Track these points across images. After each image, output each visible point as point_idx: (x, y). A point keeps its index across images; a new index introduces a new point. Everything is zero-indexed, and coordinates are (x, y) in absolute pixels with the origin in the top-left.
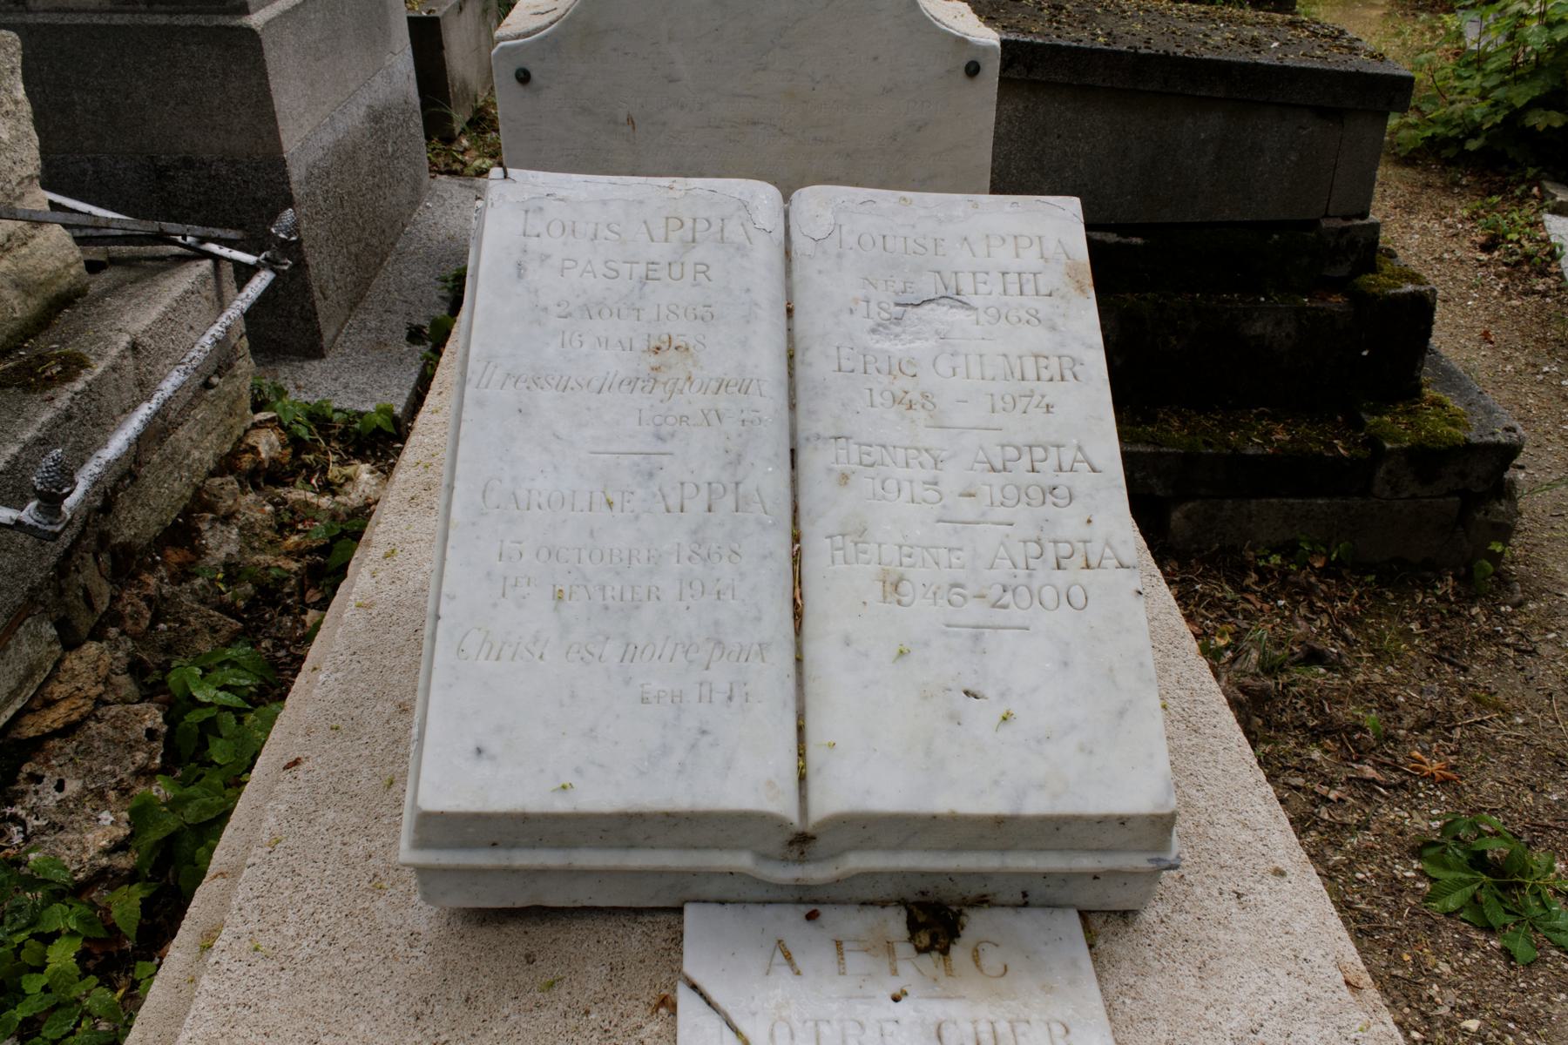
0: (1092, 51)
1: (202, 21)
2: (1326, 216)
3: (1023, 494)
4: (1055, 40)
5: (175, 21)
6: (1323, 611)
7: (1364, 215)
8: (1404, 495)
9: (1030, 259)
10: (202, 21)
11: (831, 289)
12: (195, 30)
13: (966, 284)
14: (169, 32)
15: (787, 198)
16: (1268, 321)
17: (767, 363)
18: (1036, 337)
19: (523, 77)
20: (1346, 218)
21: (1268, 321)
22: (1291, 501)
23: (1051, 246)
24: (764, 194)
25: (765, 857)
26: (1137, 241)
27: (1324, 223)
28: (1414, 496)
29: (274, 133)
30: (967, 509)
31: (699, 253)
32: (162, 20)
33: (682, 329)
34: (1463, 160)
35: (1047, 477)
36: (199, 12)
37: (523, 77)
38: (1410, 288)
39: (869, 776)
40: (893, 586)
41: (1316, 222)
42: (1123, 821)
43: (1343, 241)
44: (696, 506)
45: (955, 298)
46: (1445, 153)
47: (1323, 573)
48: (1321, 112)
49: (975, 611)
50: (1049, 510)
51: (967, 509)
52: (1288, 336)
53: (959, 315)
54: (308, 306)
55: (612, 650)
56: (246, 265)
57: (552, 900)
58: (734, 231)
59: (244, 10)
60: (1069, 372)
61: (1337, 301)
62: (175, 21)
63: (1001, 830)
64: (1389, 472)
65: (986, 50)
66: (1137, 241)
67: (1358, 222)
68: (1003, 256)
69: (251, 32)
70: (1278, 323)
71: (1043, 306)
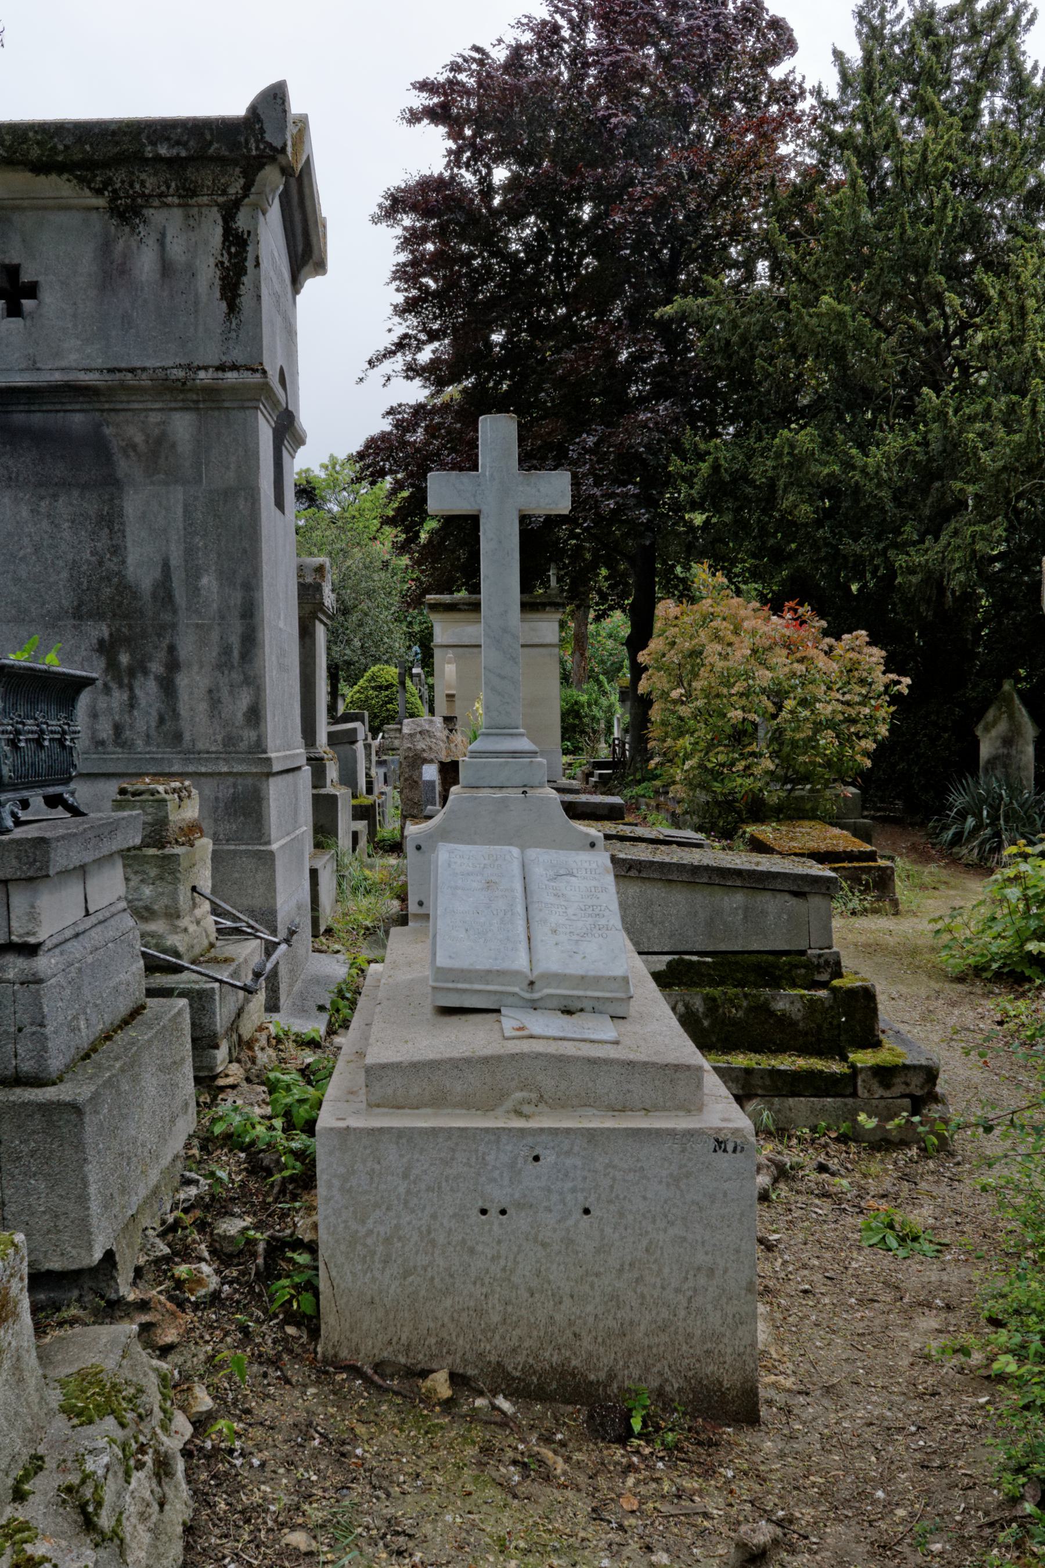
1: (250, 847)
3: (590, 915)
7: (830, 948)
9: (594, 866)
11: (538, 872)
12: (246, 852)
14: (235, 852)
16: (788, 1000)
18: (594, 883)
19: (419, 848)
21: (788, 1000)
24: (515, 851)
26: (709, 960)
28: (882, 1098)
29: (274, 898)
32: (233, 847)
33: (494, 879)
34: (998, 977)
35: (597, 911)
37: (419, 848)
40: (555, 932)
42: (615, 978)
43: (822, 961)
45: (572, 875)
46: (985, 975)
47: (837, 1140)
48: (796, 894)
49: (575, 937)
58: (508, 857)
61: (823, 993)
63: (583, 980)
66: (709, 960)
70: (792, 1003)
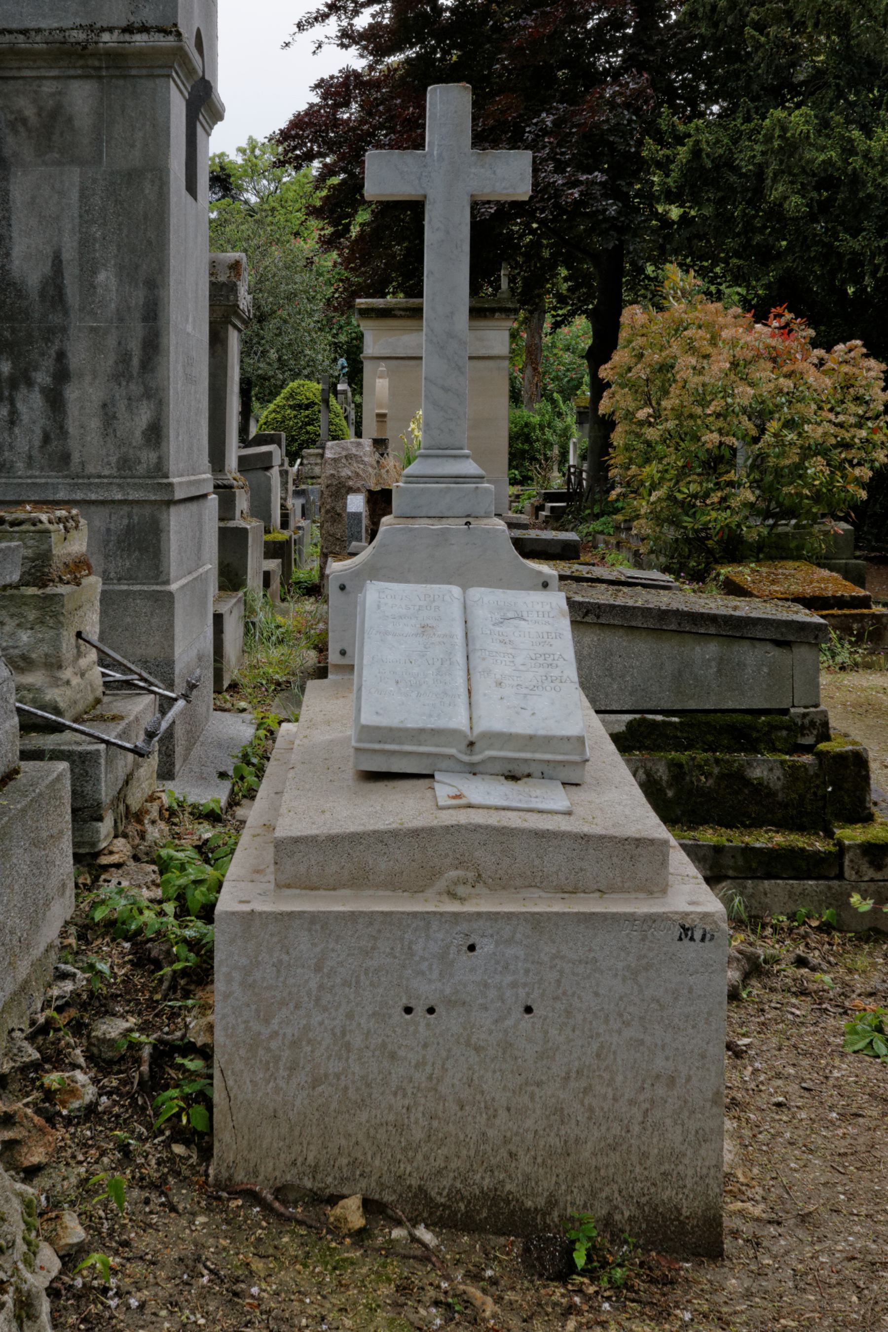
0: (634, 608)
1: (145, 588)
2: (793, 706)
3: (541, 665)
4: (612, 602)
5: (131, 588)
6: (815, 948)
7: (816, 706)
8: (866, 879)
9: (547, 608)
10: (145, 588)
11: (482, 616)
12: (140, 592)
13: (525, 615)
14: (128, 593)
15: (464, 592)
16: (764, 768)
17: (459, 632)
18: (547, 628)
19: (343, 588)
20: (806, 707)
21: (764, 768)
22: (791, 882)
23: (554, 605)
24: (456, 590)
25: (460, 752)
26: (676, 719)
27: (792, 710)
30: (522, 668)
31: (436, 604)
32: (125, 587)
35: (550, 661)
36: (144, 584)
37: (343, 588)
38: (850, 748)
39: (495, 717)
41: (788, 710)
42: (569, 739)
43: (806, 721)
44: (438, 664)
47: (819, 929)
48: (778, 643)
49: (525, 691)
50: (550, 669)
51: (522, 668)
52: (779, 779)
53: (523, 622)
54: (171, 747)
55: (414, 695)
56: (171, 698)
57: (395, 769)
59: (167, 582)
60: (559, 636)
62: (131, 588)
64: (851, 861)
65: (551, 576)
66: (676, 719)
67: (812, 709)
68: (538, 607)
69: (170, 594)
70: (771, 770)
71: (551, 620)
